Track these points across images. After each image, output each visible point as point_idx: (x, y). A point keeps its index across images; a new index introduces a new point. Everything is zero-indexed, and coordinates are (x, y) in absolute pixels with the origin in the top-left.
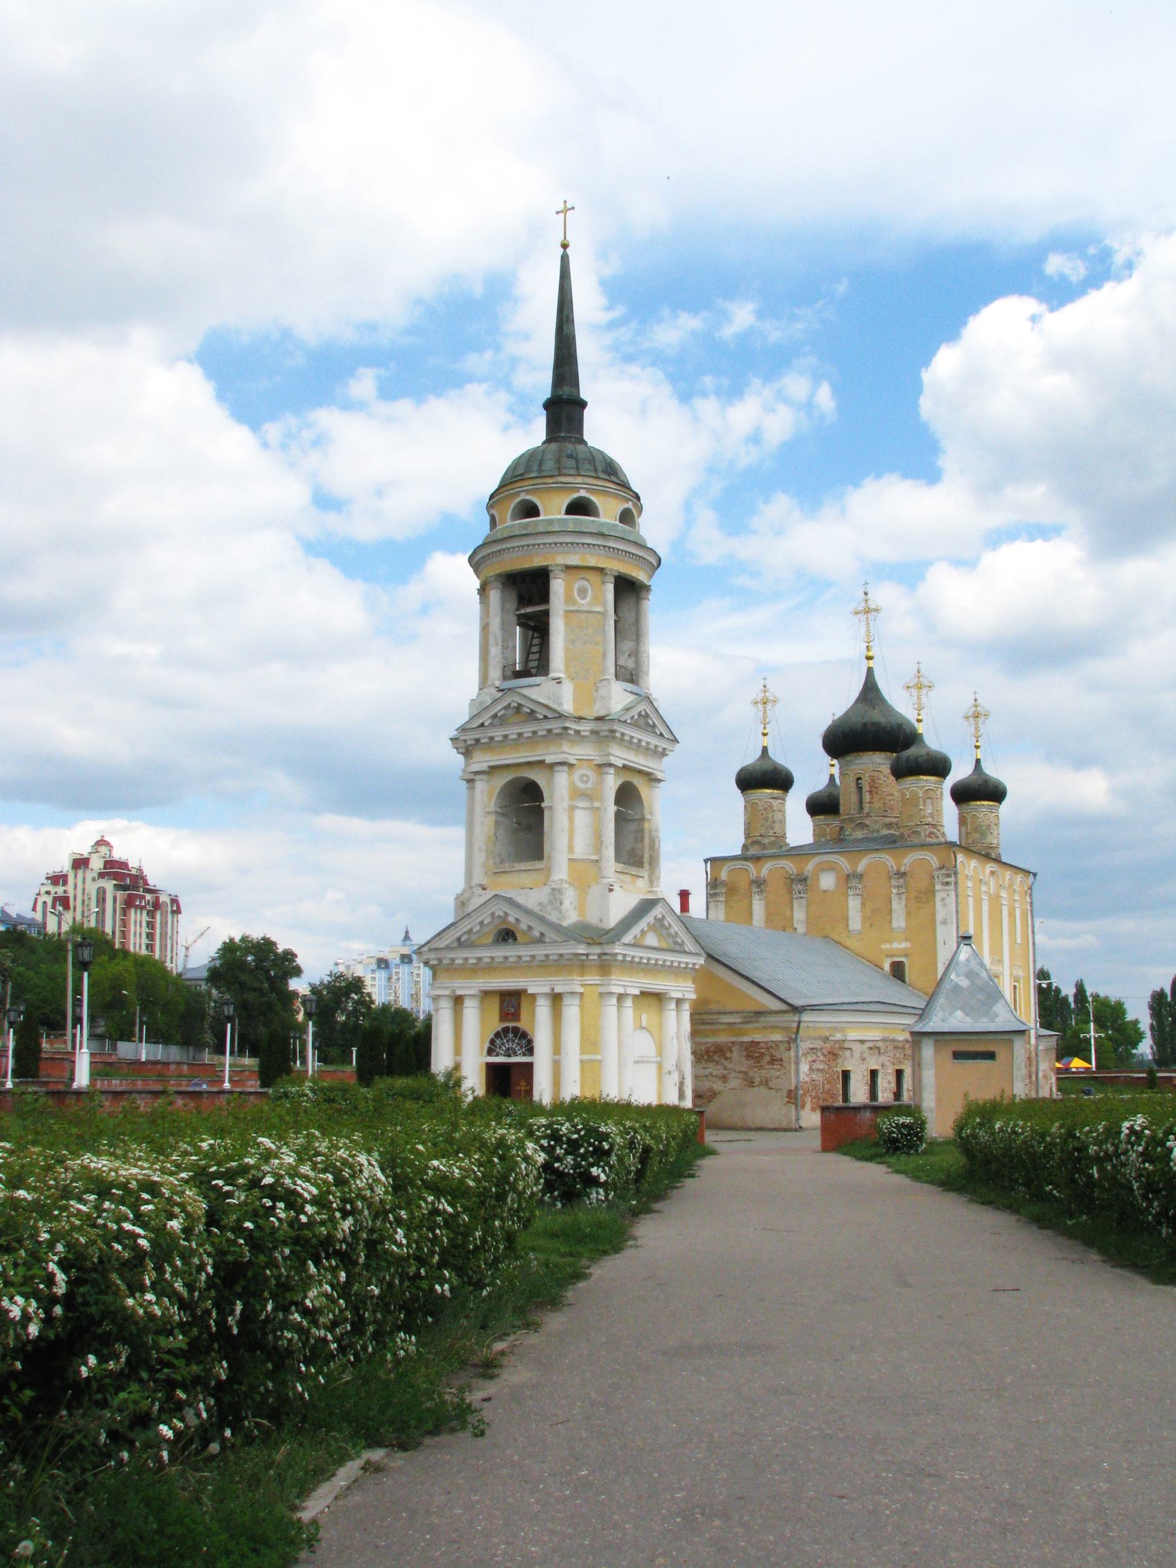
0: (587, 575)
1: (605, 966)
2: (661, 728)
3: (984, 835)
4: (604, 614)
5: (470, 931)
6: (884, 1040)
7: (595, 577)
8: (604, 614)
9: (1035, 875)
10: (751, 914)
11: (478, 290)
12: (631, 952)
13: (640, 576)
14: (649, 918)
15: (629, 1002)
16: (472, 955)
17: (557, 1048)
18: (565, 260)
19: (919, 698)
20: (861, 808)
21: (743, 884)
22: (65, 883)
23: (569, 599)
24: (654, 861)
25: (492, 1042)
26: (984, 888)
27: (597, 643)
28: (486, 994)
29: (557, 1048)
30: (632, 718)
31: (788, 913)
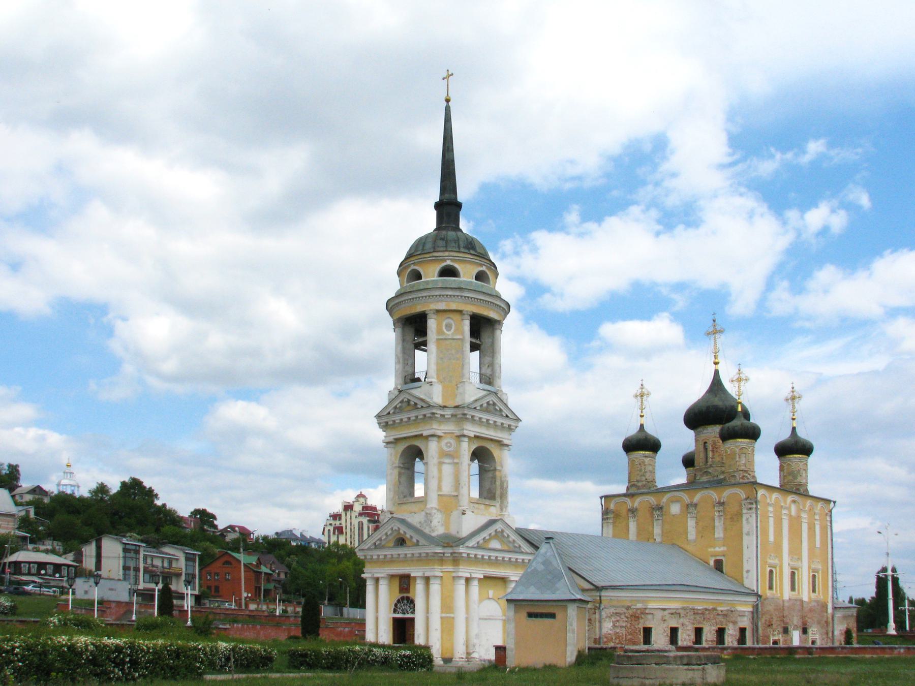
0: (451, 315)
1: (456, 560)
2: (506, 412)
3: (795, 477)
4: (462, 340)
5: (380, 539)
6: (683, 608)
7: (457, 317)
8: (462, 340)
9: (834, 502)
10: (628, 530)
11: (648, 147)
12: (473, 552)
13: (493, 315)
14: (491, 530)
15: (475, 587)
16: (382, 553)
17: (427, 611)
18: (448, 110)
19: (739, 387)
20: (707, 462)
21: (623, 512)
22: (340, 519)
23: (439, 332)
24: (503, 496)
25: (396, 605)
26: (784, 512)
27: (458, 359)
28: (392, 577)
29: (427, 611)
30: (481, 405)
31: (651, 529)
